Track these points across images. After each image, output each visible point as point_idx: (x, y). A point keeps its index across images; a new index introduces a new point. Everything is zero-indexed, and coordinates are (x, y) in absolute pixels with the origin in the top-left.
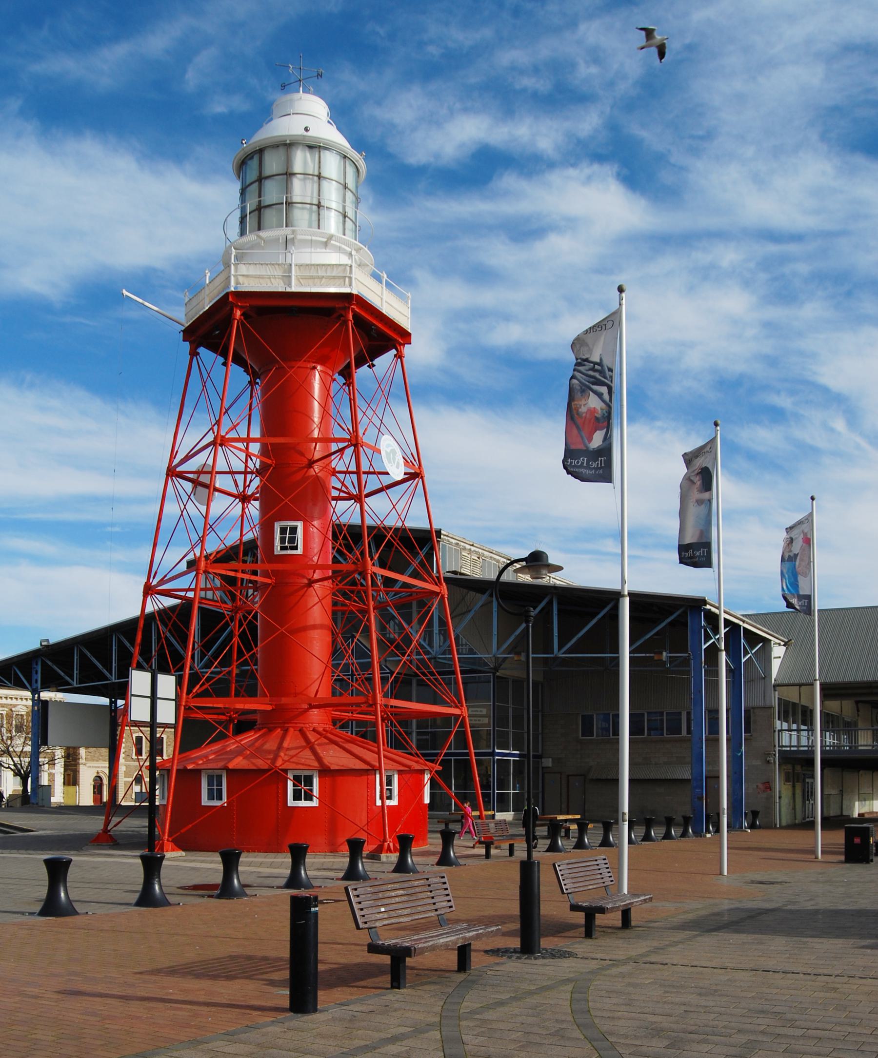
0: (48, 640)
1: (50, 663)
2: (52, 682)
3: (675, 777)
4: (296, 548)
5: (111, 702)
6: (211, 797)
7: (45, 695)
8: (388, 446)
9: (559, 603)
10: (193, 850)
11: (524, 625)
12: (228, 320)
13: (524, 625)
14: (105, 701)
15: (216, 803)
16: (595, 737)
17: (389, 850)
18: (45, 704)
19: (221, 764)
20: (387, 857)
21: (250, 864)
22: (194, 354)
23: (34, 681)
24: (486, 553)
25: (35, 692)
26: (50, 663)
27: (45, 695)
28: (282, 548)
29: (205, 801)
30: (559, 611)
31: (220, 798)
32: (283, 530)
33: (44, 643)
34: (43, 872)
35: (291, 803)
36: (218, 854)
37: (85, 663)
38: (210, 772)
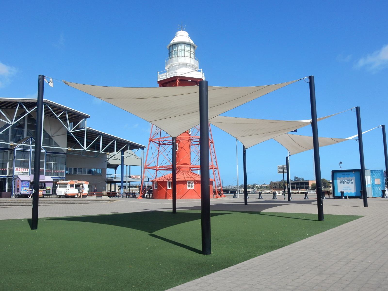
12: (176, 81)
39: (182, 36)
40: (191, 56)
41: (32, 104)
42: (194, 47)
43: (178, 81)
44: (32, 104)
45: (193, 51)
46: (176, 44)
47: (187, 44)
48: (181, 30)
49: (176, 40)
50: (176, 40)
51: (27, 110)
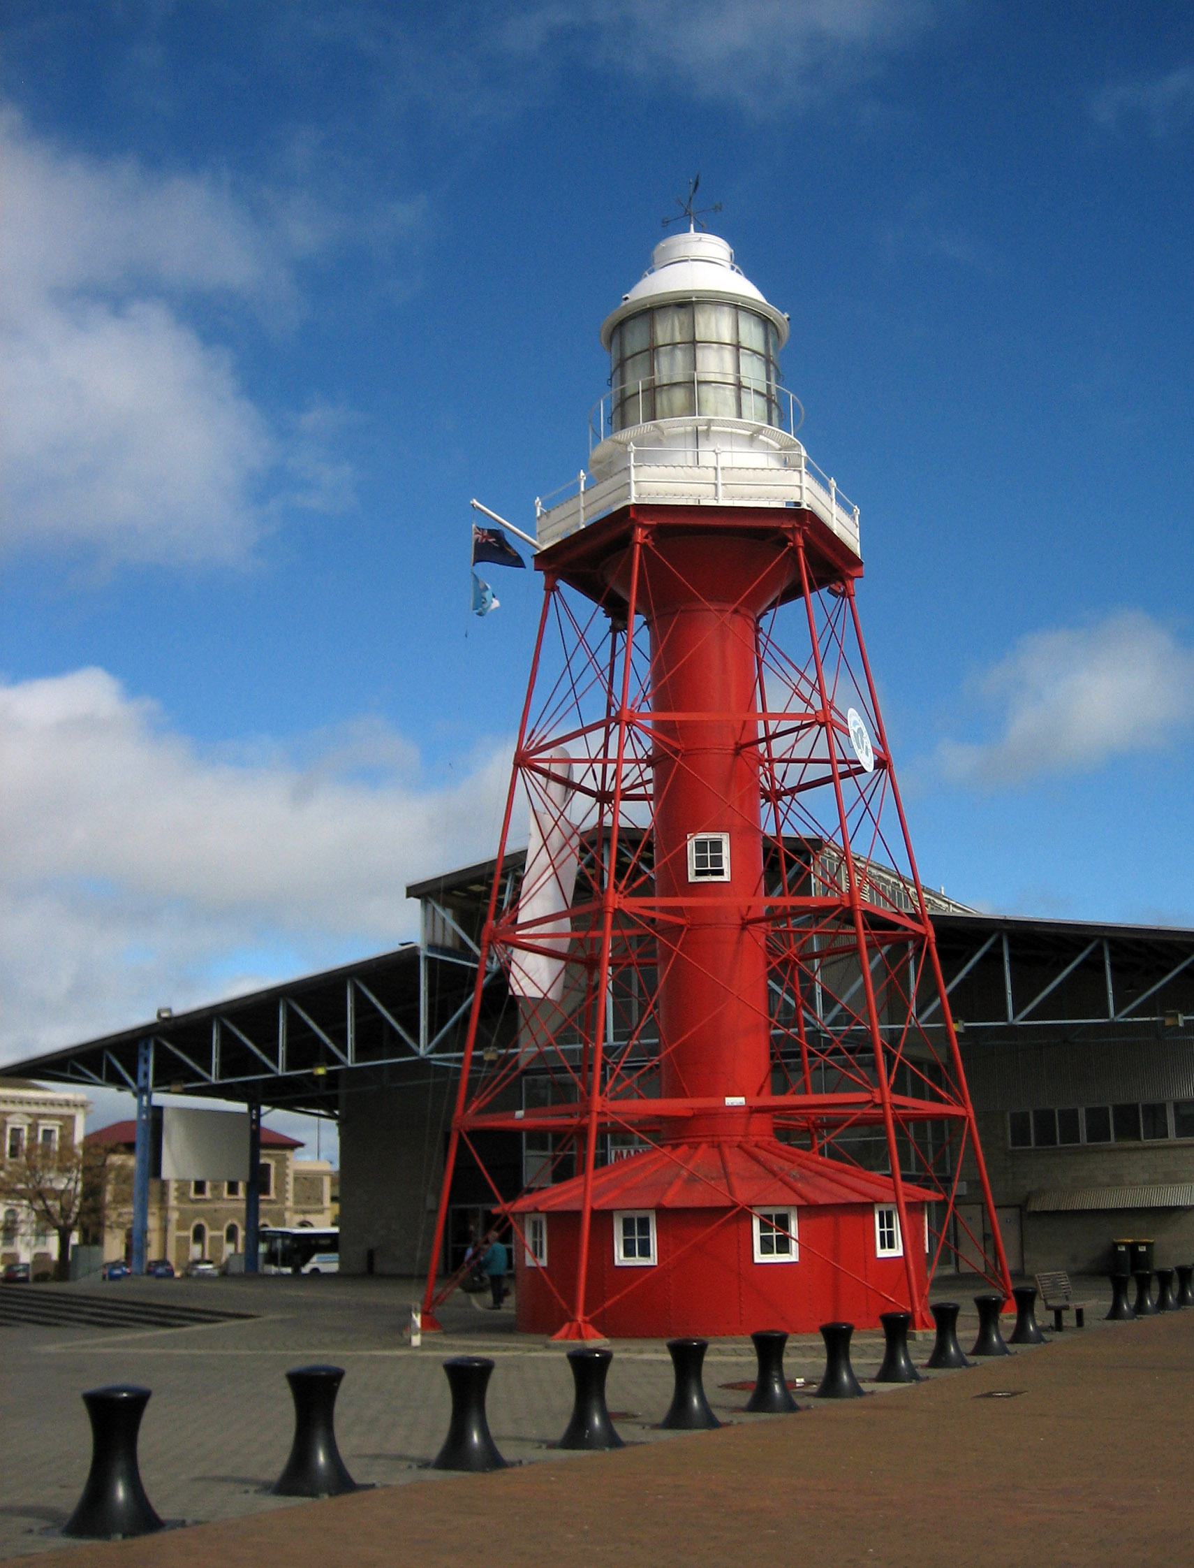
0: (169, 1010)
1: (169, 1046)
2: (171, 1074)
3: (1102, 1206)
4: (721, 873)
5: (250, 1109)
6: (629, 1252)
7: (159, 1099)
8: (855, 723)
9: (1011, 946)
10: (635, 1336)
11: (861, 979)
12: (625, 541)
13: (861, 979)
14: (243, 1107)
15: (638, 1261)
16: (1033, 1146)
17: (925, 1325)
18: (158, 1110)
19: (652, 1202)
20: (925, 1335)
21: (721, 1352)
22: (551, 588)
23: (141, 1075)
24: (874, 871)
25: (141, 1092)
26: (169, 1046)
27: (159, 1099)
28: (699, 873)
29: (620, 1259)
30: (1011, 956)
31: (645, 1252)
32: (701, 846)
33: (165, 1015)
34: (566, 1374)
35: (759, 1258)
36: (662, 1345)
37: (232, 1050)
38: (628, 1214)
39: (701, 263)
40: (738, 379)
41: (276, 1099)
42: (765, 322)
43: (640, 534)
44: (276, 1099)
45: (758, 345)
46: (651, 311)
47: (738, 306)
48: (688, 231)
49: (665, 281)
50: (665, 281)
51: (1112, 1136)
